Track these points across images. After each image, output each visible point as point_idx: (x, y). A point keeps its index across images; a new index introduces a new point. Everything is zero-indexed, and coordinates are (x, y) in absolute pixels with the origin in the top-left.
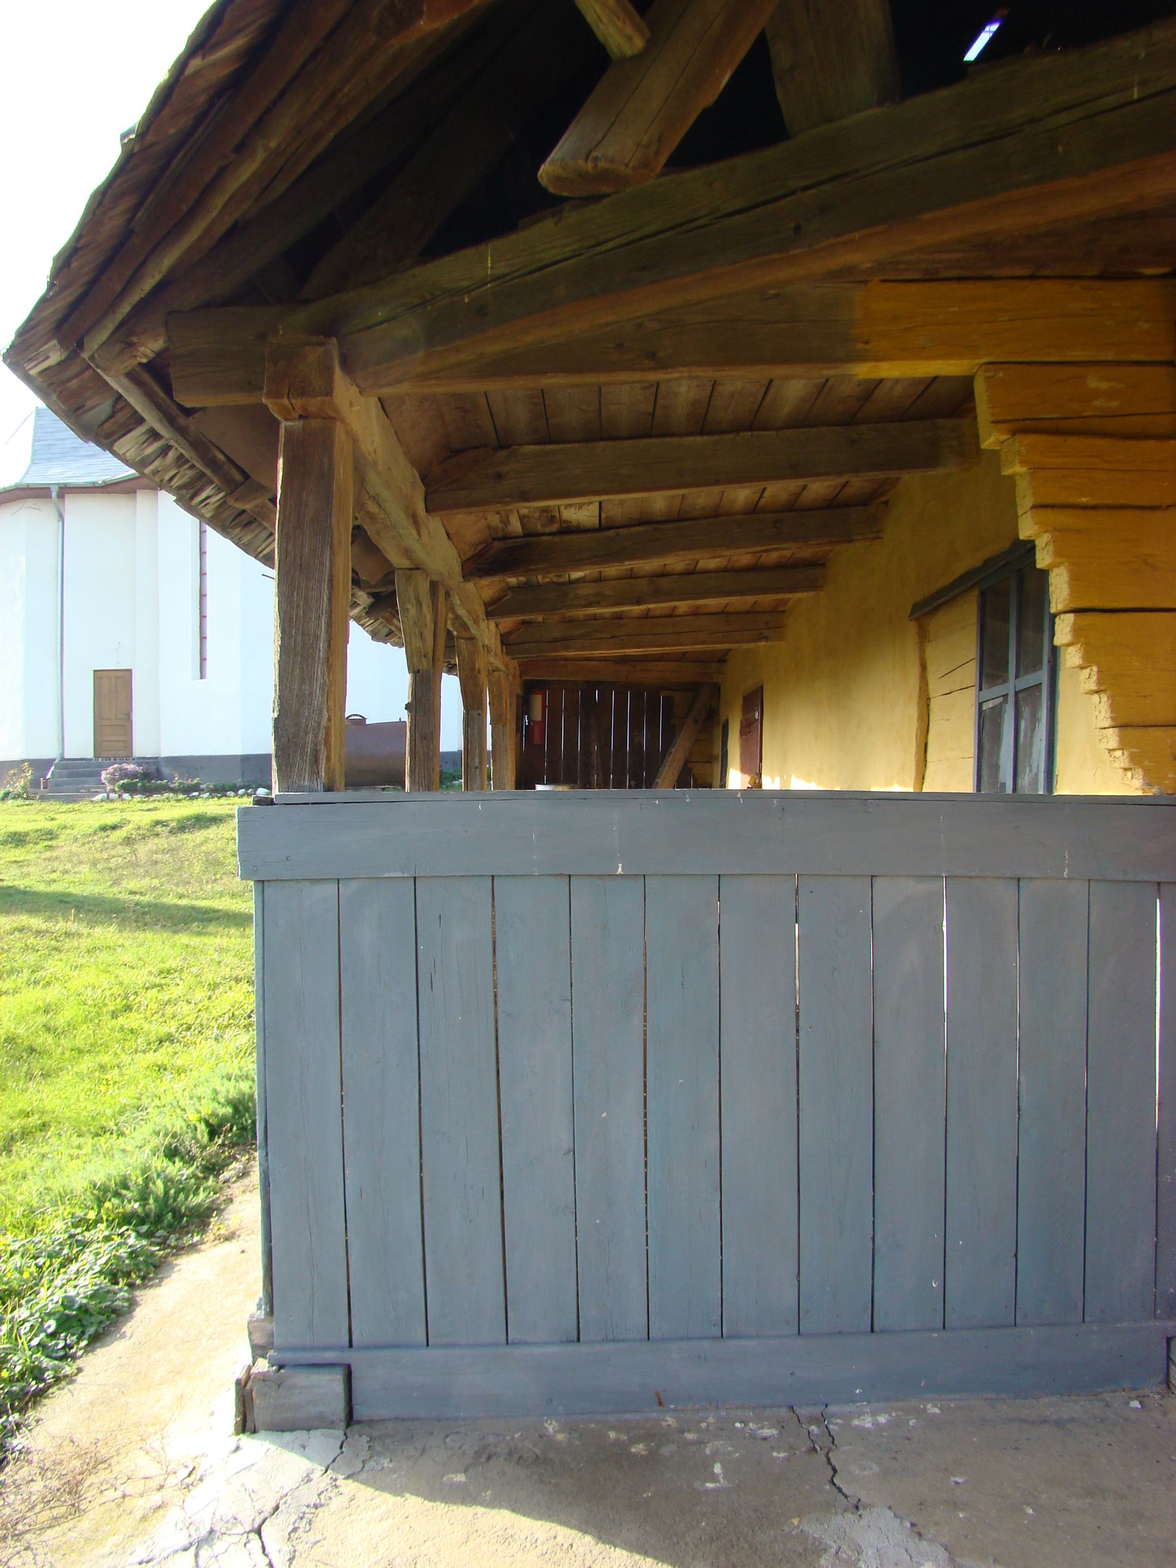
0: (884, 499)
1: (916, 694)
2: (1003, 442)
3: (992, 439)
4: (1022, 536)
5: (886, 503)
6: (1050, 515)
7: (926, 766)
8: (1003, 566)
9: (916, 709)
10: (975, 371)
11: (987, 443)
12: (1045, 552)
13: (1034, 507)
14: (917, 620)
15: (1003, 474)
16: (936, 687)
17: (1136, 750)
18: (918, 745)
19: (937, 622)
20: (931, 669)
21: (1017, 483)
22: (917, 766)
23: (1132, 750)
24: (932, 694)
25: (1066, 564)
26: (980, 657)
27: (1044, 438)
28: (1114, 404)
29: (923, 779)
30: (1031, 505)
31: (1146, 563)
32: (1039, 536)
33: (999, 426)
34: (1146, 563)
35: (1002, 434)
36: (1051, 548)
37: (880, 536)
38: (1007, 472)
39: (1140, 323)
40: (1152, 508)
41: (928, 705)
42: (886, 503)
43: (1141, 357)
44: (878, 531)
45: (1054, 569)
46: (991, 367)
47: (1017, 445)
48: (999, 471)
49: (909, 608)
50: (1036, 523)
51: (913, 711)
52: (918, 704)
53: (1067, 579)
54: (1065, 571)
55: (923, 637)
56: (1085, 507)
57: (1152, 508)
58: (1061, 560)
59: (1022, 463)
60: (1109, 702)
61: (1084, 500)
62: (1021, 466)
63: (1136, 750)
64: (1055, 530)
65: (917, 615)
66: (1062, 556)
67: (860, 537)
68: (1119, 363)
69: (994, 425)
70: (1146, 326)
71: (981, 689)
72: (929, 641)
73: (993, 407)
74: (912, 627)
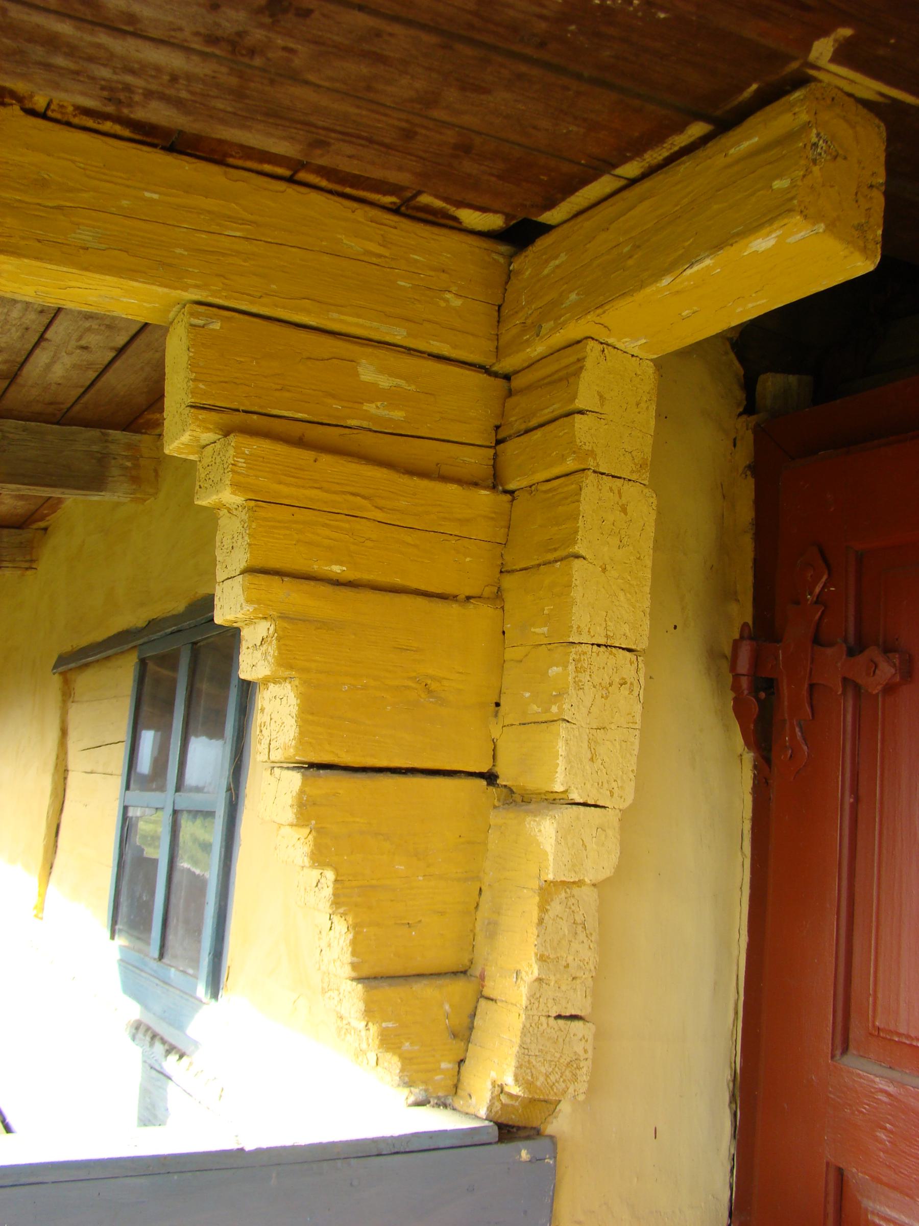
0: (42, 524)
1: (51, 767)
2: (204, 447)
3: (186, 438)
4: (221, 617)
5: (45, 529)
6: (280, 590)
7: (55, 852)
8: (172, 633)
9: (50, 780)
10: (171, 315)
11: (176, 444)
12: (258, 654)
13: (250, 571)
14: (61, 673)
15: (196, 503)
16: (76, 761)
17: (390, 1025)
18: (48, 827)
19: (84, 681)
20: (73, 735)
21: (221, 522)
22: (46, 851)
23: (384, 1025)
24: (71, 766)
25: (296, 682)
26: (134, 720)
27: (281, 449)
28: (398, 414)
29: (51, 868)
30: (243, 565)
31: (430, 692)
32: (250, 622)
33: (203, 415)
34: (430, 692)
35: (208, 430)
36: (272, 649)
37: (34, 566)
38: (205, 501)
39: (448, 296)
40: (443, 597)
41: (65, 779)
42: (45, 529)
43: (445, 350)
44: (32, 561)
45: (271, 686)
46: (202, 309)
47: (231, 452)
48: (190, 496)
49: (53, 661)
50: (249, 601)
51: (46, 783)
52: (53, 775)
53: (294, 710)
54: (292, 695)
55: (67, 695)
56: (337, 583)
57: (443, 597)
58: (287, 673)
59: (237, 486)
60: (350, 936)
61: (337, 569)
62: (233, 493)
63: (390, 1025)
64: (283, 617)
65: (61, 669)
66: (291, 667)
67: (10, 565)
68: (410, 351)
69: (193, 410)
70: (457, 303)
71: (128, 787)
72: (73, 702)
73: (194, 380)
74: (56, 681)
